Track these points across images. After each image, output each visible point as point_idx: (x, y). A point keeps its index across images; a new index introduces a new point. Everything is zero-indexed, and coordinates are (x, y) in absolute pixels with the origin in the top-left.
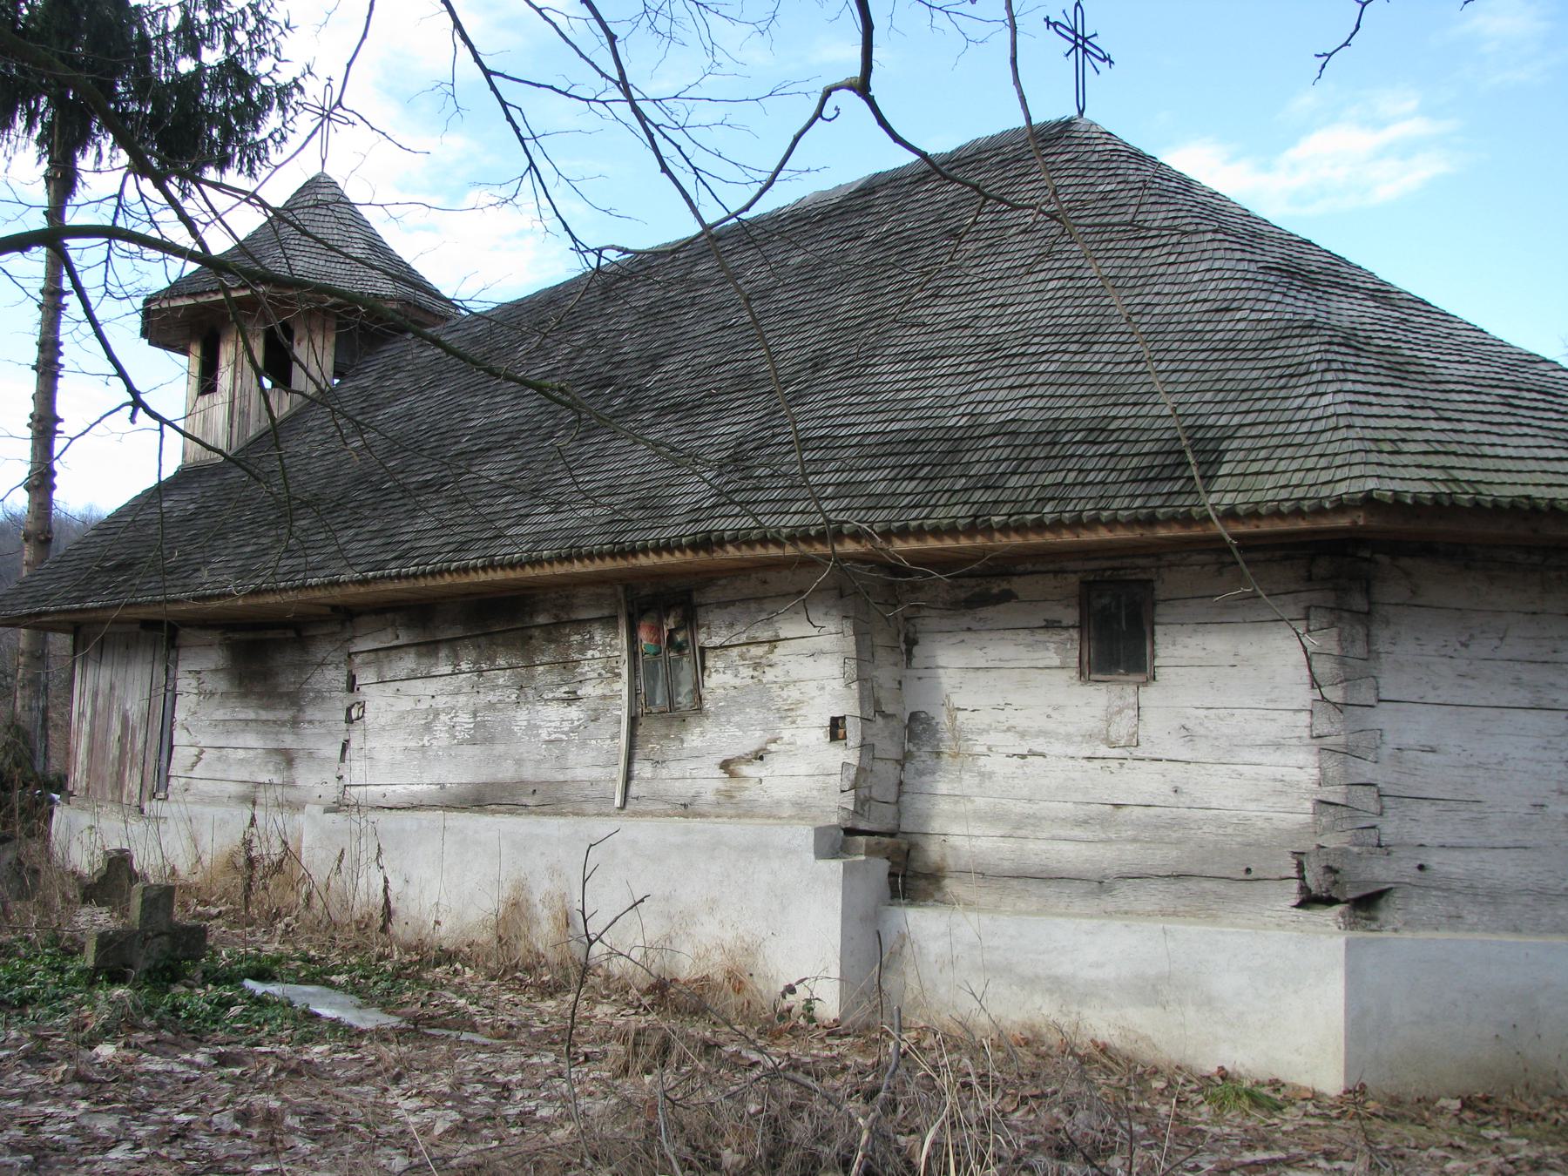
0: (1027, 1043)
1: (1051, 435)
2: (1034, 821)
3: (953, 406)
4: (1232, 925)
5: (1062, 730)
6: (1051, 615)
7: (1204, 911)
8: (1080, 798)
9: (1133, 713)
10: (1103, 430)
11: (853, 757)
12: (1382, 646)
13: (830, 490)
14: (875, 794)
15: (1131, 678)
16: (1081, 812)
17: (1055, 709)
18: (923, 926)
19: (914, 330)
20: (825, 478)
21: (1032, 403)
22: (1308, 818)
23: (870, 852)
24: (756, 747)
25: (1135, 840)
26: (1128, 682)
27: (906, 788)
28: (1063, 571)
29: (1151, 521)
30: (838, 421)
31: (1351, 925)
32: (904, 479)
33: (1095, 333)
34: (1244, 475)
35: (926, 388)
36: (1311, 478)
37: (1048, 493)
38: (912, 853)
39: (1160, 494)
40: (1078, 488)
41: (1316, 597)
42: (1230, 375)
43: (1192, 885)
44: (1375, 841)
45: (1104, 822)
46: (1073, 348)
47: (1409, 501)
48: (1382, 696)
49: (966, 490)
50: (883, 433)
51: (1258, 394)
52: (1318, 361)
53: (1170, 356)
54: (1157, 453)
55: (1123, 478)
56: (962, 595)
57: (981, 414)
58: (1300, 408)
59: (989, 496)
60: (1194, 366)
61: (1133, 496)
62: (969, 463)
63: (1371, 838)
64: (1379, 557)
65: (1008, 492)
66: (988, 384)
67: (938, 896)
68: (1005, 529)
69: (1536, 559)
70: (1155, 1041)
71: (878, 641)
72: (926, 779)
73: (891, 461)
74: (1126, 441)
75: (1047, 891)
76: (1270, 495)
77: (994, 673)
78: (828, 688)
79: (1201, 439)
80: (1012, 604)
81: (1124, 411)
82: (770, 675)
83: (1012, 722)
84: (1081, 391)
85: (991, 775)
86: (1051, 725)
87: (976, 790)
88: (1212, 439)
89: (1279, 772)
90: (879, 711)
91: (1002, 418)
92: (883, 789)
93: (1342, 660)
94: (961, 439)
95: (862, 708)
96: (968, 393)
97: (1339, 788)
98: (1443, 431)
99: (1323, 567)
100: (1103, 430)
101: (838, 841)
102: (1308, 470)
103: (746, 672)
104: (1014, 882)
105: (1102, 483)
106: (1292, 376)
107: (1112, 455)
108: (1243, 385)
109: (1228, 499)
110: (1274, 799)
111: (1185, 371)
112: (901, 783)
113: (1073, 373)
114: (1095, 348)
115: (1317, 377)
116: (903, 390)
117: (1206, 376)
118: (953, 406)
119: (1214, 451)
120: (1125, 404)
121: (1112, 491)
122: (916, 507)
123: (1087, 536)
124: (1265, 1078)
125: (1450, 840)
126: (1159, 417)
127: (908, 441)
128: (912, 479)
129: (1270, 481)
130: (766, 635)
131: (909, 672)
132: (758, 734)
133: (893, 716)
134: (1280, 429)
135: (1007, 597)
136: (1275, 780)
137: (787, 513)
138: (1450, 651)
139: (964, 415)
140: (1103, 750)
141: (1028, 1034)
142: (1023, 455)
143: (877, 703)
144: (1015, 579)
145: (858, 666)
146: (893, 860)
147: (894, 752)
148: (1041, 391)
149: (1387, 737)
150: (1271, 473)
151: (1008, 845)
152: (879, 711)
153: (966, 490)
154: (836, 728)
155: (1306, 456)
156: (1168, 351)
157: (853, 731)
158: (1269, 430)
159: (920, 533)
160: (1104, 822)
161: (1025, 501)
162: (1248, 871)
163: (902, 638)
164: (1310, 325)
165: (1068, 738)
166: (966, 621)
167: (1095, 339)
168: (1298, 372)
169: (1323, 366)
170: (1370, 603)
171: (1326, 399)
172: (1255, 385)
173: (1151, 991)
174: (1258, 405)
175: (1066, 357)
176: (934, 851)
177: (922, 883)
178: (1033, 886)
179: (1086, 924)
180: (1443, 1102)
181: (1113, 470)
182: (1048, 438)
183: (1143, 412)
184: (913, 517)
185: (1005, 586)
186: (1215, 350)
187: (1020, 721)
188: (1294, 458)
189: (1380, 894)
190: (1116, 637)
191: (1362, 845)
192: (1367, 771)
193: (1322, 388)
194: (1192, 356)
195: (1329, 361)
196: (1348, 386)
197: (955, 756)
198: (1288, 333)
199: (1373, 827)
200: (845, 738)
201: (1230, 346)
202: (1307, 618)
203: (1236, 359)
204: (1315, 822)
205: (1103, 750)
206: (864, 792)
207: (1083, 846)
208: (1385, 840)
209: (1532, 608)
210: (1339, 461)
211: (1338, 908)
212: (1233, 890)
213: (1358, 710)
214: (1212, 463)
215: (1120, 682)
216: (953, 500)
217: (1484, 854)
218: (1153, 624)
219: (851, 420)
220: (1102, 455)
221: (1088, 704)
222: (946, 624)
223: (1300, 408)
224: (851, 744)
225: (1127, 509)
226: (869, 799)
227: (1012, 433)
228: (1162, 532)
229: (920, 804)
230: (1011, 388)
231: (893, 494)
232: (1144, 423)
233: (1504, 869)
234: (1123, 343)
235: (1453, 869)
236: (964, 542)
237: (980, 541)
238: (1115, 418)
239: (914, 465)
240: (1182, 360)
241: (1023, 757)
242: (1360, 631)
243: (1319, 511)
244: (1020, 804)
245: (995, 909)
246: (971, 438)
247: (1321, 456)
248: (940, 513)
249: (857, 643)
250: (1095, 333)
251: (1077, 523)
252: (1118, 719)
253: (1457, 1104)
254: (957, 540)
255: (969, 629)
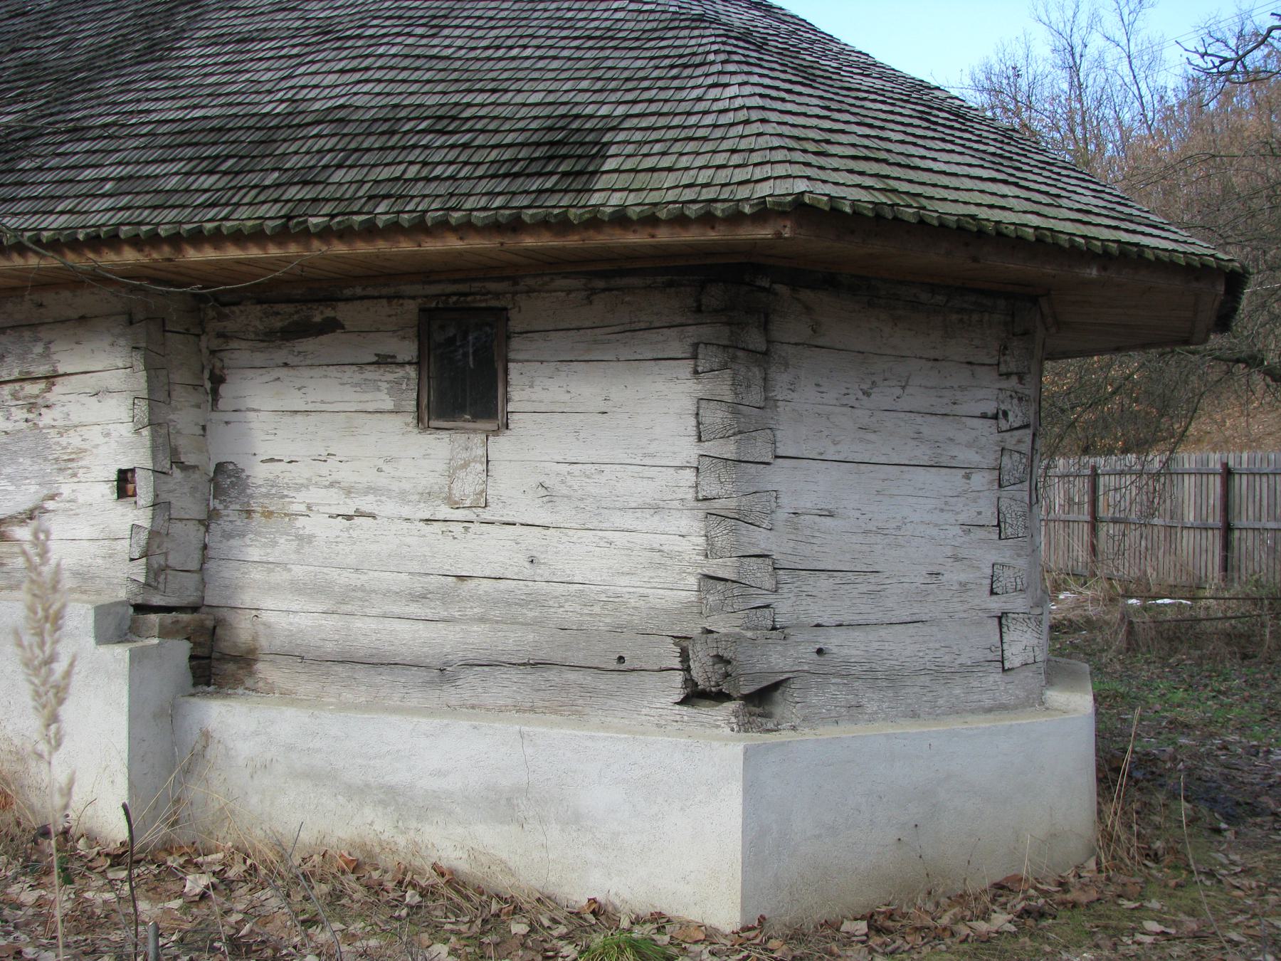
0: (356, 867)
1: (388, 124)
2: (364, 594)
3: (270, 92)
4: (604, 726)
5: (395, 486)
6: (385, 349)
7: (566, 707)
8: (415, 567)
9: (480, 467)
10: (454, 118)
11: (143, 518)
12: (779, 393)
13: (109, 186)
14: (173, 561)
15: (480, 425)
16: (418, 585)
17: (386, 461)
18: (228, 719)
19: (233, 13)
20: (105, 172)
21: (367, 88)
22: (693, 597)
23: (165, 633)
24: (30, 505)
25: (482, 620)
26: (475, 431)
27: (211, 553)
28: (399, 297)
29: (516, 225)
30: (128, 108)
31: (745, 727)
32: (202, 173)
33: (445, 17)
34: (635, 171)
35: (239, 72)
36: (722, 176)
37: (383, 189)
38: (218, 630)
39: (527, 192)
40: (420, 184)
41: (706, 332)
42: (609, 63)
43: (552, 675)
44: (769, 623)
45: (445, 597)
46: (419, 31)
47: (848, 210)
48: (780, 452)
49: (278, 186)
50: (182, 120)
51: (646, 84)
52: (716, 52)
53: (535, 42)
54: (523, 145)
55: (480, 172)
56: (278, 324)
57: (303, 100)
58: (699, 99)
59: (307, 193)
60: (566, 53)
61: (492, 194)
62: (284, 154)
63: (765, 618)
64: (776, 286)
65: (331, 188)
66: (314, 68)
67: (249, 682)
68: (325, 234)
69: (940, 299)
70: (510, 864)
71: (176, 377)
72: (235, 542)
73: (189, 152)
74: (483, 131)
75: (378, 679)
76: (671, 196)
77: (313, 417)
78: (114, 434)
79: (578, 130)
80: (338, 334)
81: (480, 99)
82: (47, 418)
83: (335, 477)
84: (428, 76)
85: (310, 539)
86: (382, 481)
87: (293, 557)
88: (592, 130)
89: (656, 541)
90: (177, 463)
91: (329, 104)
92: (182, 555)
93: (735, 409)
94: (277, 127)
95: (154, 458)
96: (290, 77)
97: (729, 561)
98: (867, 136)
99: (715, 296)
100: (454, 118)
101: (126, 621)
102: (718, 167)
103: (19, 414)
104: (339, 668)
105: (452, 178)
106: (685, 66)
107: (465, 146)
108: (626, 74)
109: (616, 199)
110: (648, 573)
111: (555, 58)
112: (205, 547)
113: (418, 57)
114: (446, 32)
115: (717, 68)
116: (212, 74)
117: (580, 64)
118: (270, 92)
119: (596, 144)
120: (481, 91)
121: (465, 187)
122: (213, 205)
123: (432, 245)
124: (645, 911)
125: (847, 618)
126: (524, 105)
127: (212, 130)
128: (211, 173)
129: (671, 179)
130: (42, 370)
131: (214, 415)
132: (33, 488)
133: (195, 467)
134: (677, 121)
135: (332, 326)
136: (652, 550)
137: (51, 212)
138: (852, 402)
139: (282, 101)
140: (444, 511)
141: (357, 855)
142: (353, 146)
143: (174, 452)
144: (341, 305)
145: (151, 409)
146: (194, 640)
147: (197, 511)
148: (378, 75)
149: (784, 500)
150: (670, 169)
151: (331, 622)
152: (177, 463)
153: (278, 186)
154: (124, 483)
155: (714, 152)
156: (533, 36)
157: (144, 487)
158: (662, 121)
159: (217, 239)
160: (445, 597)
161: (352, 199)
162: (621, 659)
163: (206, 375)
164: (701, 18)
165: (403, 497)
166: (281, 355)
167: (446, 22)
168: (689, 63)
169: (723, 57)
170: (769, 342)
171: (732, 91)
172: (641, 74)
173: (504, 805)
174: (646, 95)
175: (410, 41)
176: (243, 631)
177: (230, 667)
178: (361, 673)
179: (425, 723)
180: (847, 926)
181: (466, 163)
182: (385, 127)
183: (503, 100)
184: (208, 219)
185: (329, 313)
186: (589, 38)
187: (345, 474)
188: (698, 154)
189: (776, 686)
190: (462, 383)
191: (755, 628)
192: (761, 540)
193: (725, 79)
194: (562, 43)
195: (729, 53)
196: (755, 79)
197: (268, 514)
198: (676, 24)
199: (767, 606)
200: (134, 495)
201: (608, 35)
202: (695, 357)
203: (615, 48)
204: (700, 601)
205: (444, 511)
206: (158, 561)
207: (421, 625)
208: (780, 621)
209: (933, 354)
210: (756, 157)
211: (731, 706)
212: (603, 682)
213: (752, 469)
214: (594, 157)
215: (465, 430)
216: (262, 198)
217: (883, 632)
218: (507, 361)
219: (143, 106)
220: (452, 146)
221: (426, 456)
222: (259, 359)
223: (699, 99)
224: (141, 502)
225: (484, 209)
226: (164, 569)
227: (341, 120)
228: (529, 241)
229: (228, 572)
230: (342, 71)
231: (187, 190)
232: (506, 112)
233: (902, 647)
234: (479, 28)
235: (854, 652)
236: (274, 251)
237: (293, 249)
238: (469, 105)
239: (217, 157)
240: (551, 47)
241: (349, 518)
242: (757, 372)
243: (736, 217)
244: (345, 573)
245: (315, 703)
246: (289, 126)
247: (733, 151)
248: (243, 212)
249: (149, 380)
250: (445, 17)
251: (420, 227)
252: (462, 474)
253: (862, 926)
254: (264, 248)
255: (286, 365)
